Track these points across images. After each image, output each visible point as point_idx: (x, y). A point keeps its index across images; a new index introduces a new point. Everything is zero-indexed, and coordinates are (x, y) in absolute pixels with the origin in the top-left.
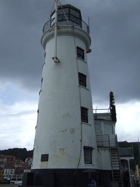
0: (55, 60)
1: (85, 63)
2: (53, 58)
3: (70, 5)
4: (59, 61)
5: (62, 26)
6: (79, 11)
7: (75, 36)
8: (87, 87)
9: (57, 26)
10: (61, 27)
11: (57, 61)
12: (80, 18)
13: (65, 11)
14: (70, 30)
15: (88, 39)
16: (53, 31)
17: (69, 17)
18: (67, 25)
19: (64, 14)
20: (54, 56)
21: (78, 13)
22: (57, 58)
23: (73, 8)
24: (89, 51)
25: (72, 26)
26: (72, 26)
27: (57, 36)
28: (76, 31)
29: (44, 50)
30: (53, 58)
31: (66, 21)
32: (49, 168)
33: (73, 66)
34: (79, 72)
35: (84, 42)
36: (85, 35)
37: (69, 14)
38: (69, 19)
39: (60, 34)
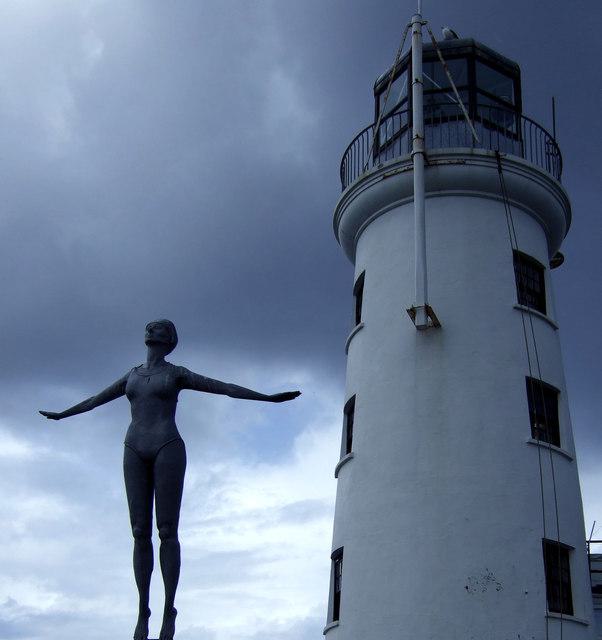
0: (421, 319)
1: (549, 330)
2: (412, 312)
3: (473, 45)
4: (437, 325)
5: (443, 155)
6: (511, 72)
7: (513, 204)
8: (564, 447)
9: (424, 154)
10: (439, 155)
11: (429, 324)
12: (516, 109)
13: (452, 75)
14: (483, 170)
15: (562, 213)
16: (409, 173)
17: (472, 106)
18: (467, 150)
19: (450, 90)
20: (415, 300)
21: (511, 82)
22: (428, 311)
23: (485, 56)
24: (557, 261)
25: (492, 153)
26: (492, 153)
27: (427, 197)
28: (511, 176)
29: (350, 263)
30: (412, 312)
31: (461, 125)
32: (152, 538)
33: (497, 347)
34: (535, 375)
35: (534, 217)
36: (548, 194)
37: (471, 89)
38: (475, 118)
39: (436, 189)
